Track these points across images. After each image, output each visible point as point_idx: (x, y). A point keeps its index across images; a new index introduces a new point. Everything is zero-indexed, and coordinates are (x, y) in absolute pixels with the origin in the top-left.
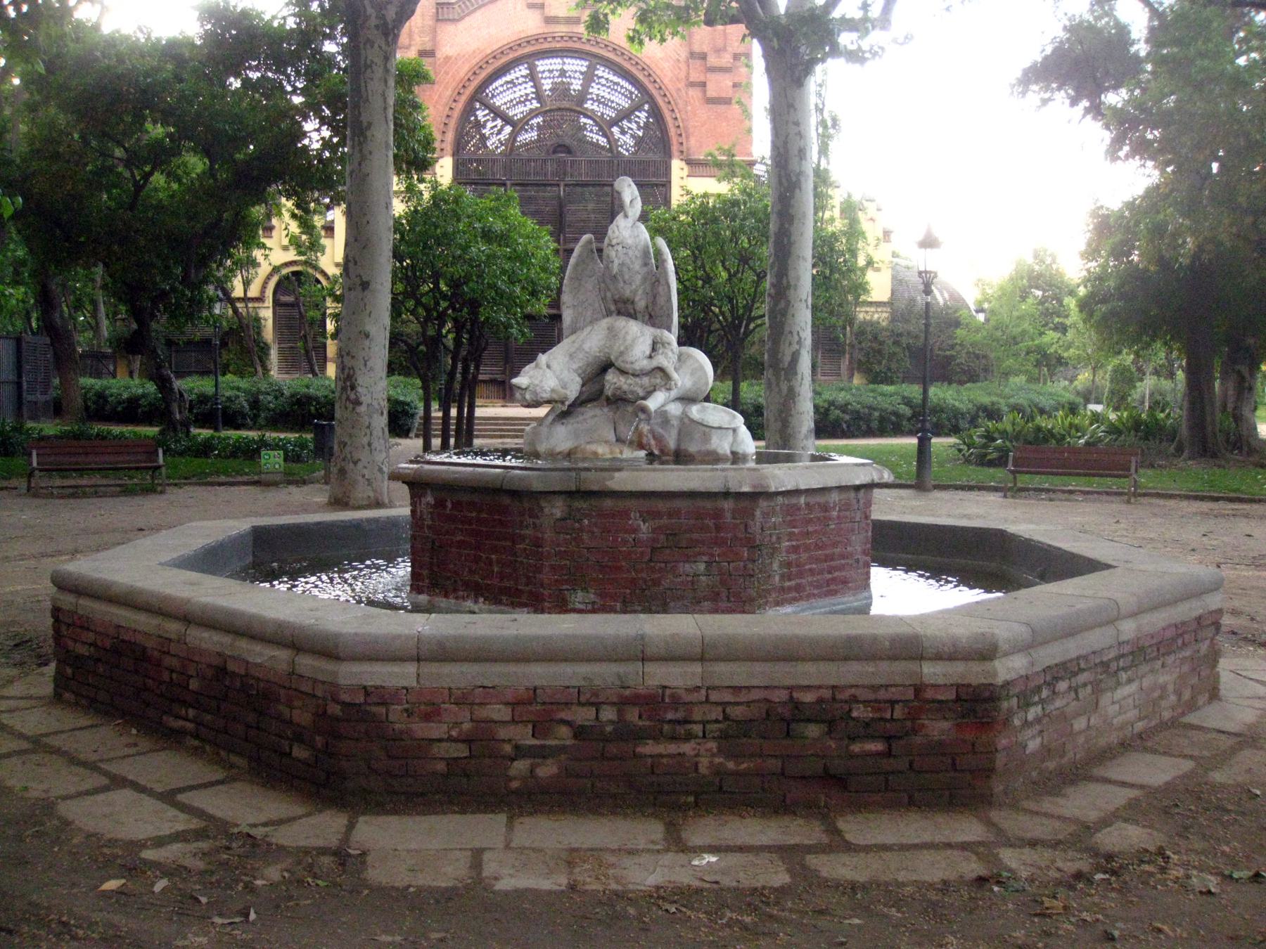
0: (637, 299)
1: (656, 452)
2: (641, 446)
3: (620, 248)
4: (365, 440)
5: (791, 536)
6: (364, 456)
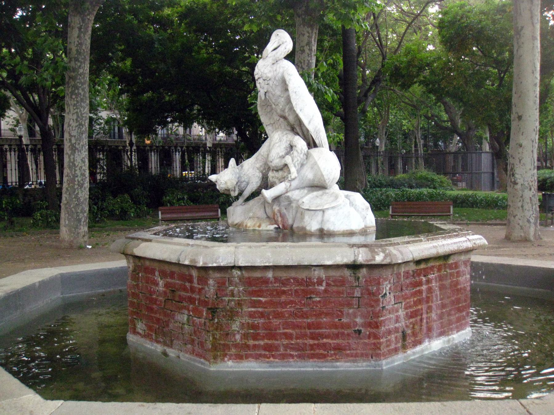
0: (287, 114)
1: (281, 227)
4: (520, 204)
5: (254, 304)
6: (519, 213)
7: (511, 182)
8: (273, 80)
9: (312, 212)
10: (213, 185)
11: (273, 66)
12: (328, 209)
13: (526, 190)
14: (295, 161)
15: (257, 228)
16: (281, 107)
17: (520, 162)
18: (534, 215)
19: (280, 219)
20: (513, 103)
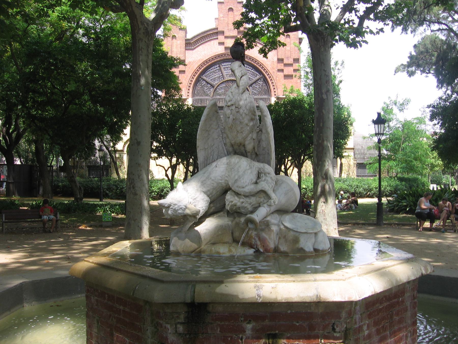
1: (261, 250)
2: (251, 246)
3: (233, 108)
8: (244, 108)
9: (308, 235)
19: (259, 243)
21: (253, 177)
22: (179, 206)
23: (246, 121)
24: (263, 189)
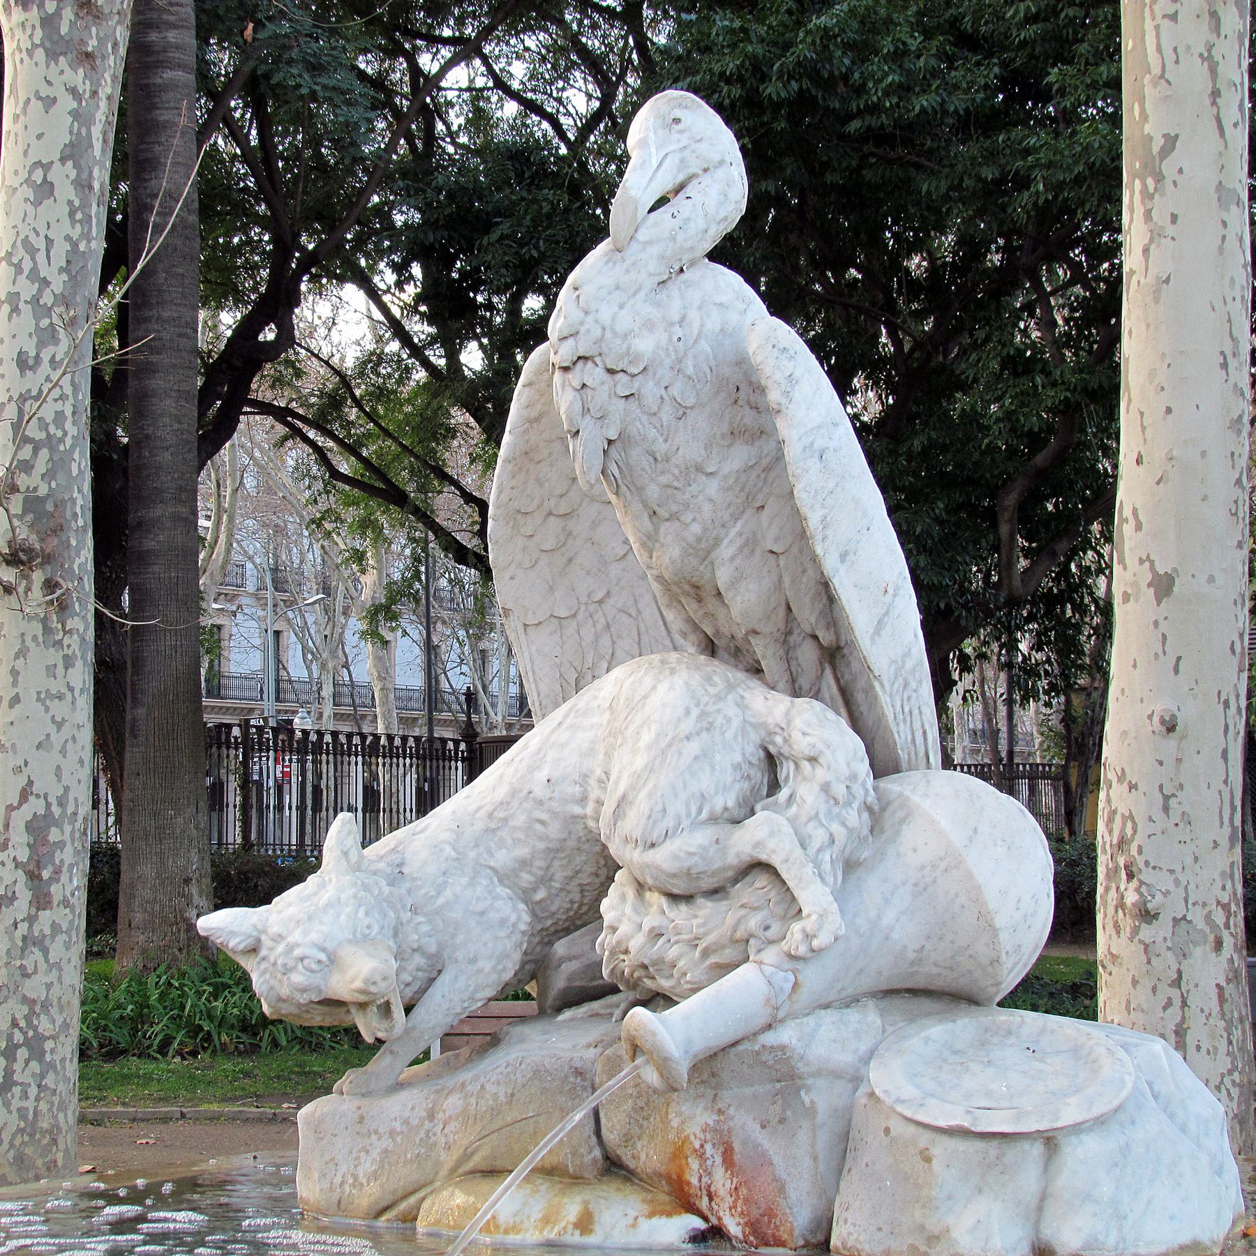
0: (723, 577)
1: (734, 1227)
7: (1121, 905)
8: (665, 374)
10: (224, 973)
11: (662, 296)
12: (1076, 1129)
13: (1198, 952)
14: (815, 845)
15: (576, 1238)
16: (696, 528)
17: (1166, 809)
18: (1236, 1076)
19: (722, 1182)
20: (1127, 512)
21: (723, 783)
22: (291, 948)
23: (688, 445)
24: (763, 857)
